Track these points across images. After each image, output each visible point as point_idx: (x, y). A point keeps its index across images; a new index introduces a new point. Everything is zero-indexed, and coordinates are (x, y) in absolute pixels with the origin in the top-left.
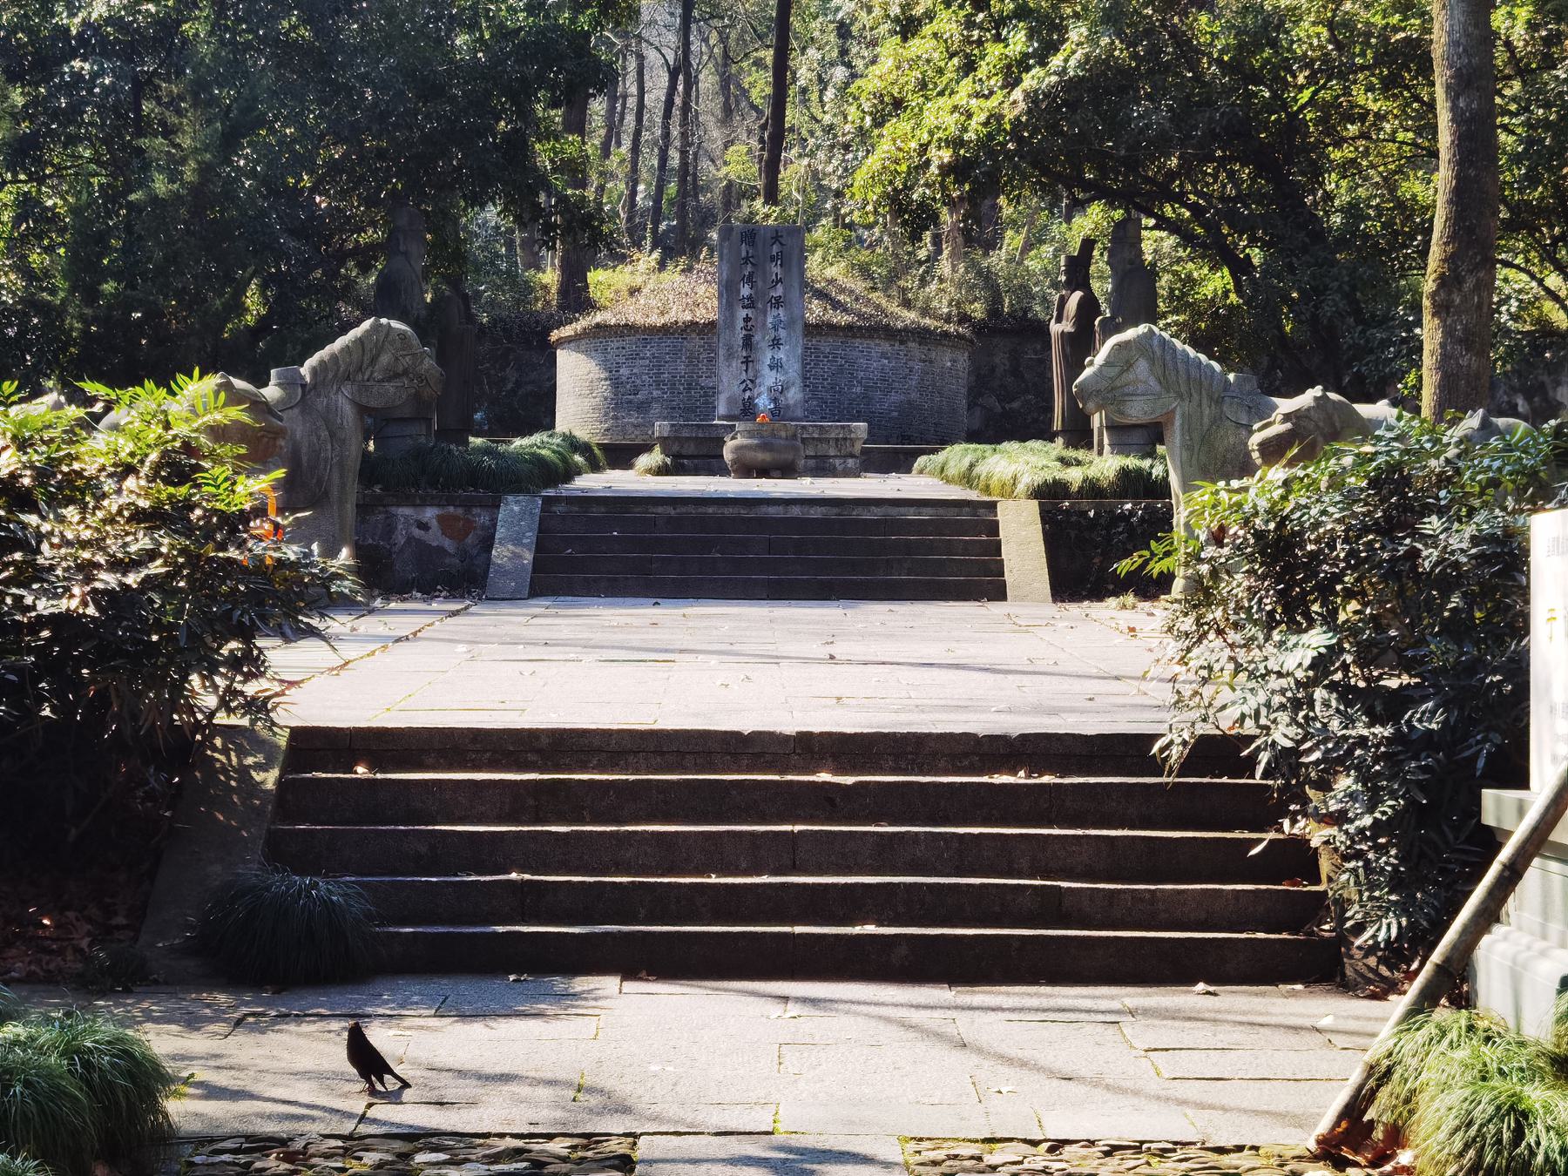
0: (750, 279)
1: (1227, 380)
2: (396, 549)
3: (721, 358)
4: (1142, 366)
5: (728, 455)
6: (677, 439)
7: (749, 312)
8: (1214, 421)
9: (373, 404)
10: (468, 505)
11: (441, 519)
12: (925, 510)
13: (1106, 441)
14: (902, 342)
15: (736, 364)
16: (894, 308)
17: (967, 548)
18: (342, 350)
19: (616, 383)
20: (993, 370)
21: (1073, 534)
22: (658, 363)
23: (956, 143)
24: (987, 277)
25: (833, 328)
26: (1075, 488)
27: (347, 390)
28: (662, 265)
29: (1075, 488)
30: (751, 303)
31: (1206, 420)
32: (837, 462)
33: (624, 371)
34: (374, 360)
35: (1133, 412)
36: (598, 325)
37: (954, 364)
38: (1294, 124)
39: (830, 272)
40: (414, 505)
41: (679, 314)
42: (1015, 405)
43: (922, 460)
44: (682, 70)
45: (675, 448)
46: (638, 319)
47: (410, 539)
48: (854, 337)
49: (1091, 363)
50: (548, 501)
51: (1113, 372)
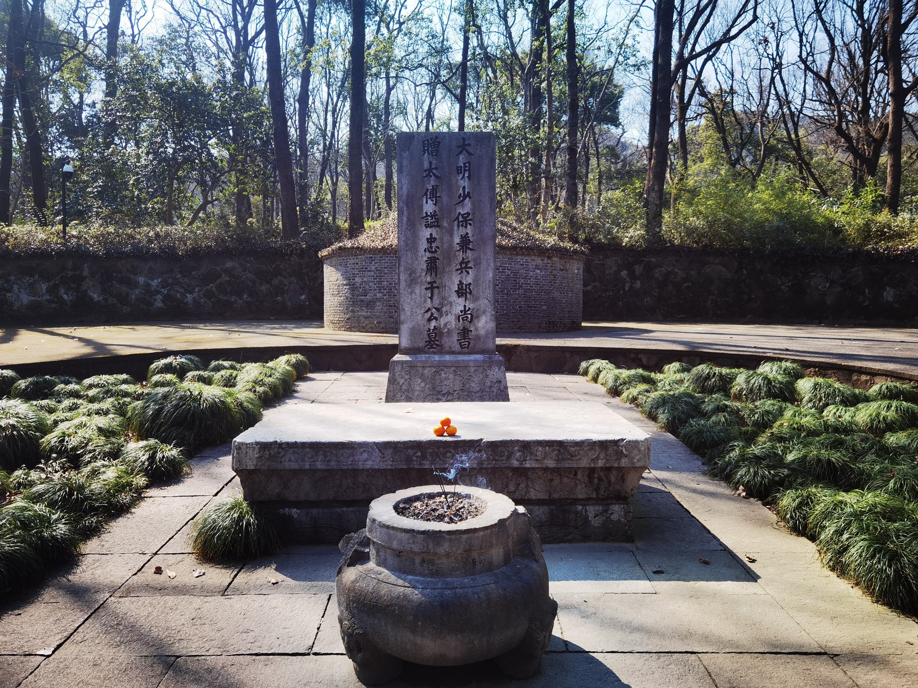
0: (434, 194)
3: (403, 285)
6: (273, 472)
7: (434, 231)
14: (549, 258)
19: (353, 287)
30: (435, 221)
32: (592, 510)
37: (576, 268)
48: (517, 255)
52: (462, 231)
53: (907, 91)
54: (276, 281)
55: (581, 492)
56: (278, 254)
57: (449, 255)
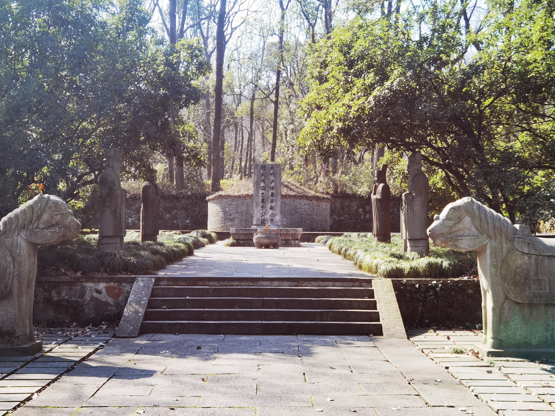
0: (264, 181)
1: (515, 229)
2: (86, 303)
4: (467, 220)
5: (255, 241)
6: (238, 234)
7: (263, 191)
8: (509, 252)
9: (38, 242)
10: (120, 281)
11: (107, 289)
12: (337, 283)
13: (408, 245)
14: (311, 200)
15: (259, 208)
16: (307, 190)
17: (360, 305)
18: (21, 212)
19: (225, 213)
20: (336, 208)
21: (408, 295)
22: (237, 206)
23: (343, 120)
24: (334, 181)
25: (290, 196)
26: (406, 272)
27: (23, 234)
28: (241, 178)
29: (406, 272)
30: (264, 188)
31: (505, 250)
32: (292, 241)
33: (227, 209)
34: (39, 218)
35: (463, 246)
36: (219, 195)
37: (326, 206)
38: (481, 116)
39: (289, 180)
40: (94, 282)
41: (244, 192)
42: (342, 218)
43: (319, 238)
44: (251, 134)
45: (237, 237)
46: (231, 193)
47: (92, 298)
48: (296, 199)
49: (438, 218)
50: (158, 280)
51: (451, 223)
52: (272, 191)
53: (413, 151)
54: (174, 213)
55: (291, 238)
56: (176, 198)
57: (268, 198)
